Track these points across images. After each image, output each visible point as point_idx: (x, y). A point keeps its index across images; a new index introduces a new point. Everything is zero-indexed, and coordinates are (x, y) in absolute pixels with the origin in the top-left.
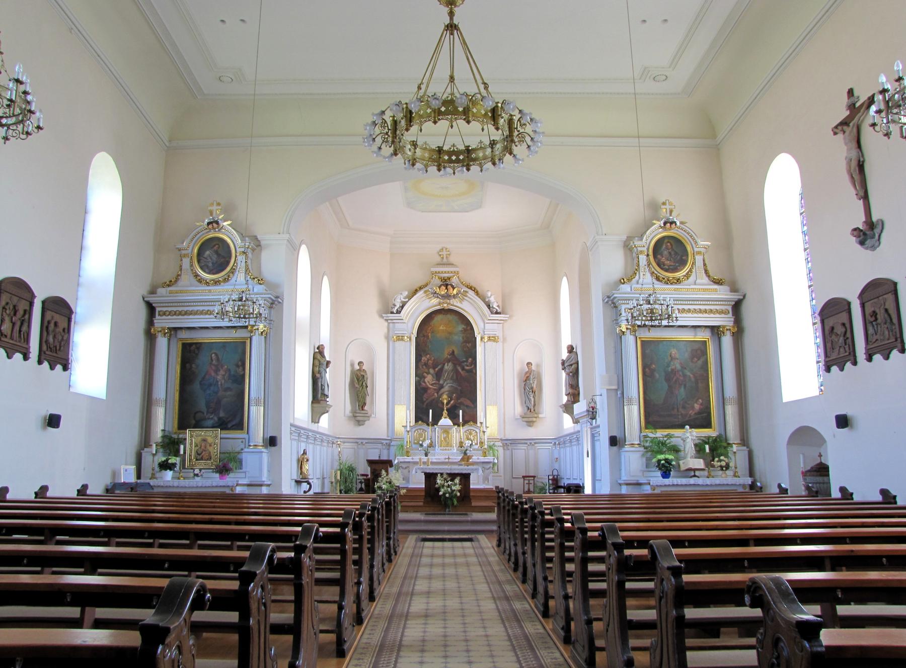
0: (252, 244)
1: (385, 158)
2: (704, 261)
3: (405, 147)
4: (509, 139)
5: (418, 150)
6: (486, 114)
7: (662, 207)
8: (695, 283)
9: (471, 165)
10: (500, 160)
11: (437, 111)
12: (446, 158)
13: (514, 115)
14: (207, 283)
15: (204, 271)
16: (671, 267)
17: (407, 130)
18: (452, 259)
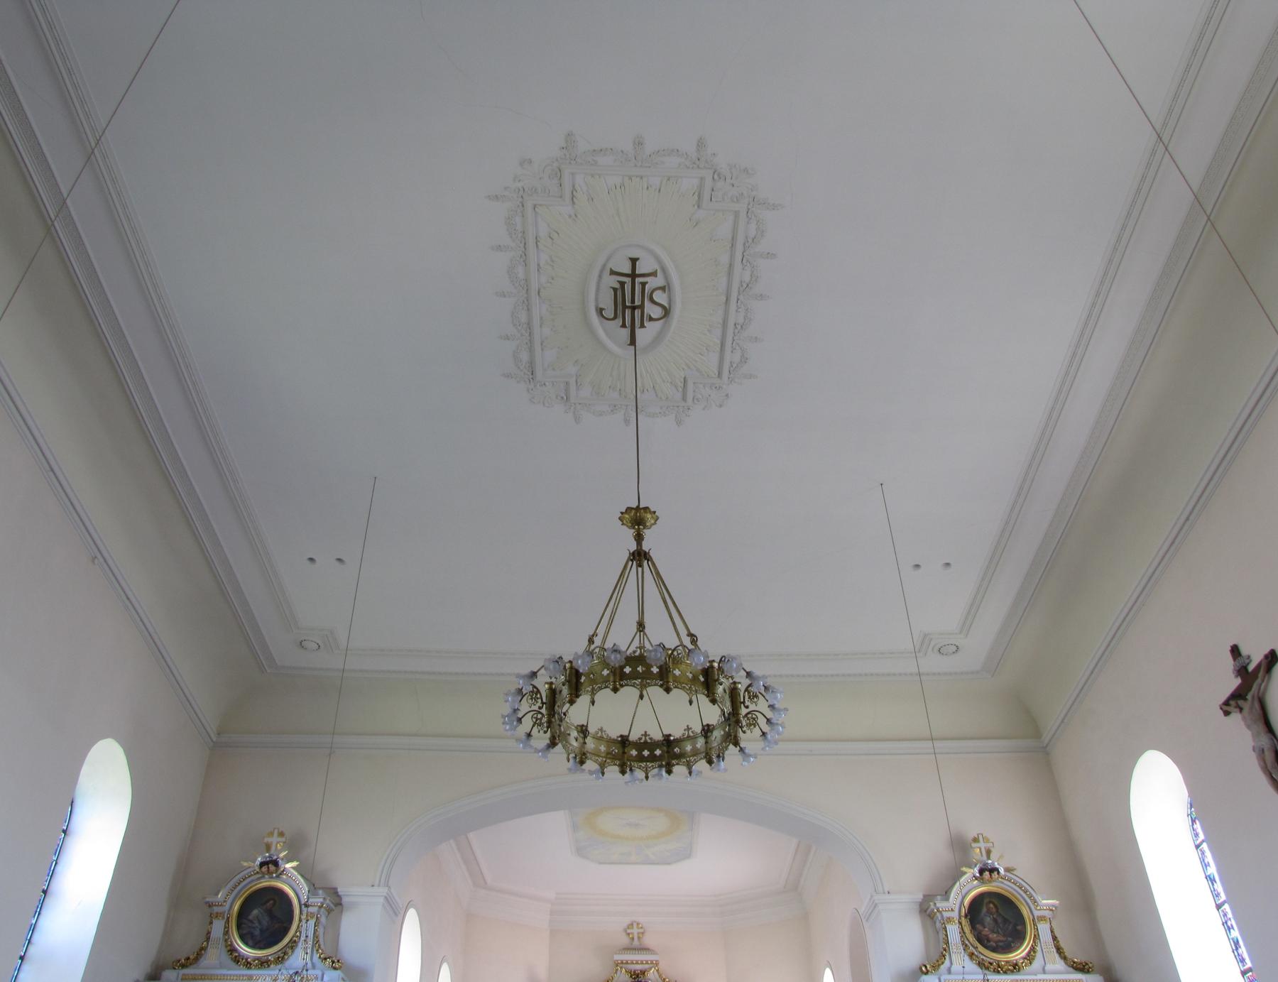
0: (328, 901)
1: (537, 751)
2: (1052, 932)
3: (569, 735)
4: (733, 719)
5: (589, 740)
6: (695, 678)
7: (974, 845)
8: (1044, 970)
9: (674, 765)
10: (718, 756)
11: (618, 671)
12: (634, 753)
13: (739, 683)
14: (248, 963)
15: (246, 943)
16: (1001, 944)
17: (572, 702)
18: (649, 941)
